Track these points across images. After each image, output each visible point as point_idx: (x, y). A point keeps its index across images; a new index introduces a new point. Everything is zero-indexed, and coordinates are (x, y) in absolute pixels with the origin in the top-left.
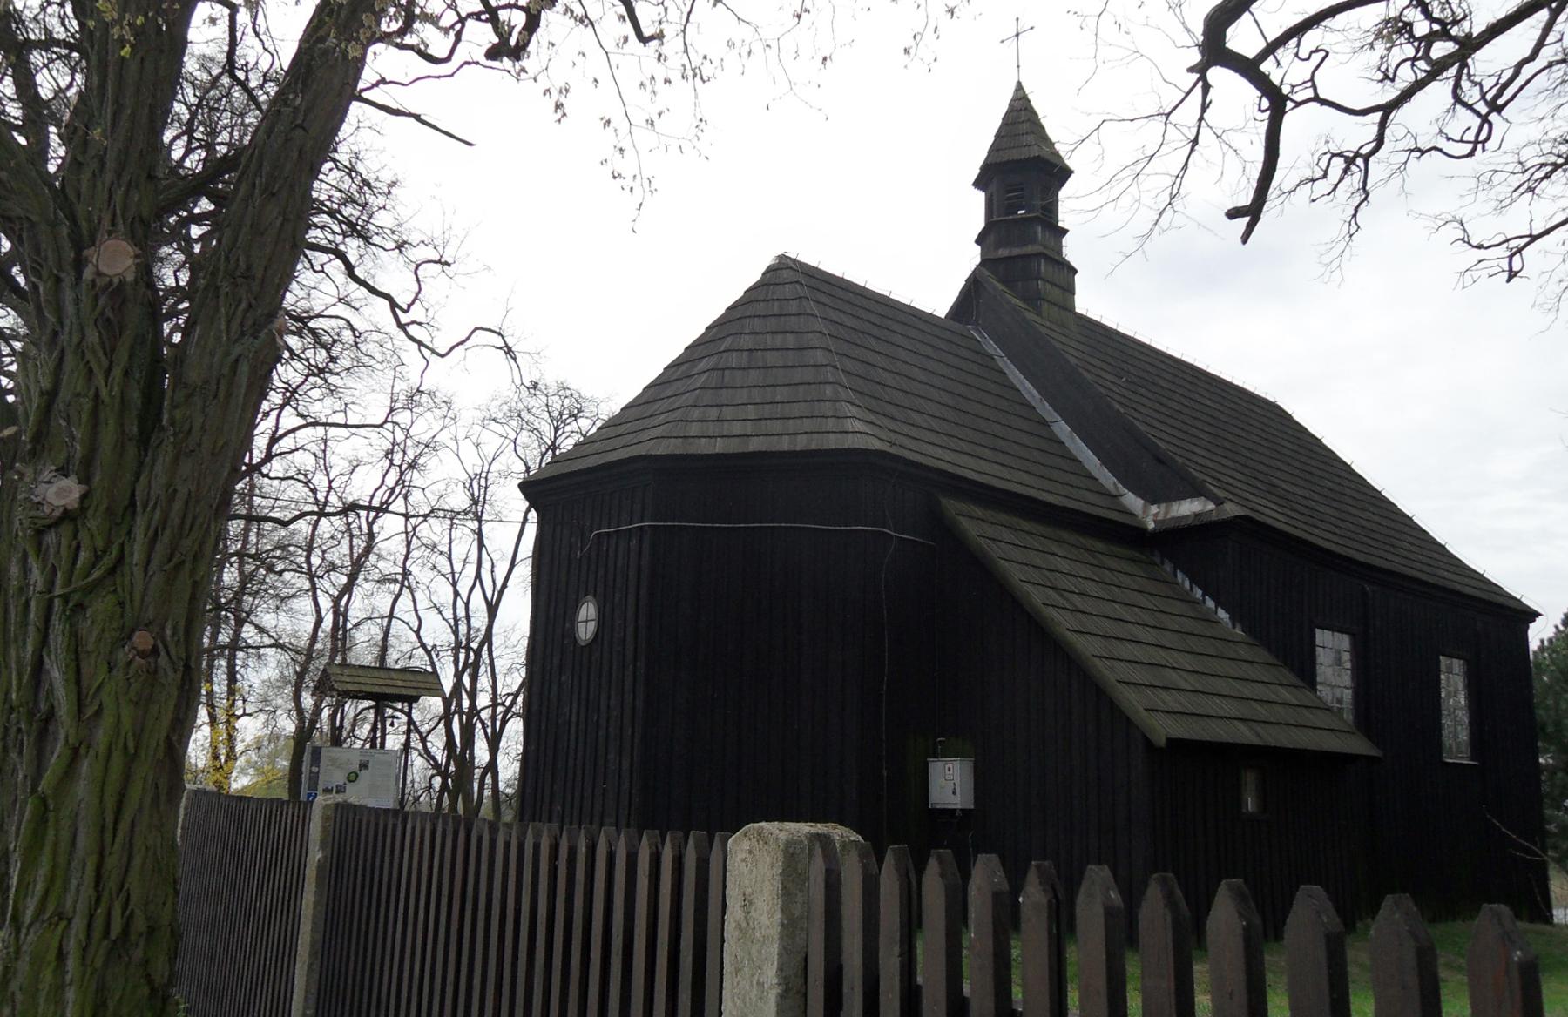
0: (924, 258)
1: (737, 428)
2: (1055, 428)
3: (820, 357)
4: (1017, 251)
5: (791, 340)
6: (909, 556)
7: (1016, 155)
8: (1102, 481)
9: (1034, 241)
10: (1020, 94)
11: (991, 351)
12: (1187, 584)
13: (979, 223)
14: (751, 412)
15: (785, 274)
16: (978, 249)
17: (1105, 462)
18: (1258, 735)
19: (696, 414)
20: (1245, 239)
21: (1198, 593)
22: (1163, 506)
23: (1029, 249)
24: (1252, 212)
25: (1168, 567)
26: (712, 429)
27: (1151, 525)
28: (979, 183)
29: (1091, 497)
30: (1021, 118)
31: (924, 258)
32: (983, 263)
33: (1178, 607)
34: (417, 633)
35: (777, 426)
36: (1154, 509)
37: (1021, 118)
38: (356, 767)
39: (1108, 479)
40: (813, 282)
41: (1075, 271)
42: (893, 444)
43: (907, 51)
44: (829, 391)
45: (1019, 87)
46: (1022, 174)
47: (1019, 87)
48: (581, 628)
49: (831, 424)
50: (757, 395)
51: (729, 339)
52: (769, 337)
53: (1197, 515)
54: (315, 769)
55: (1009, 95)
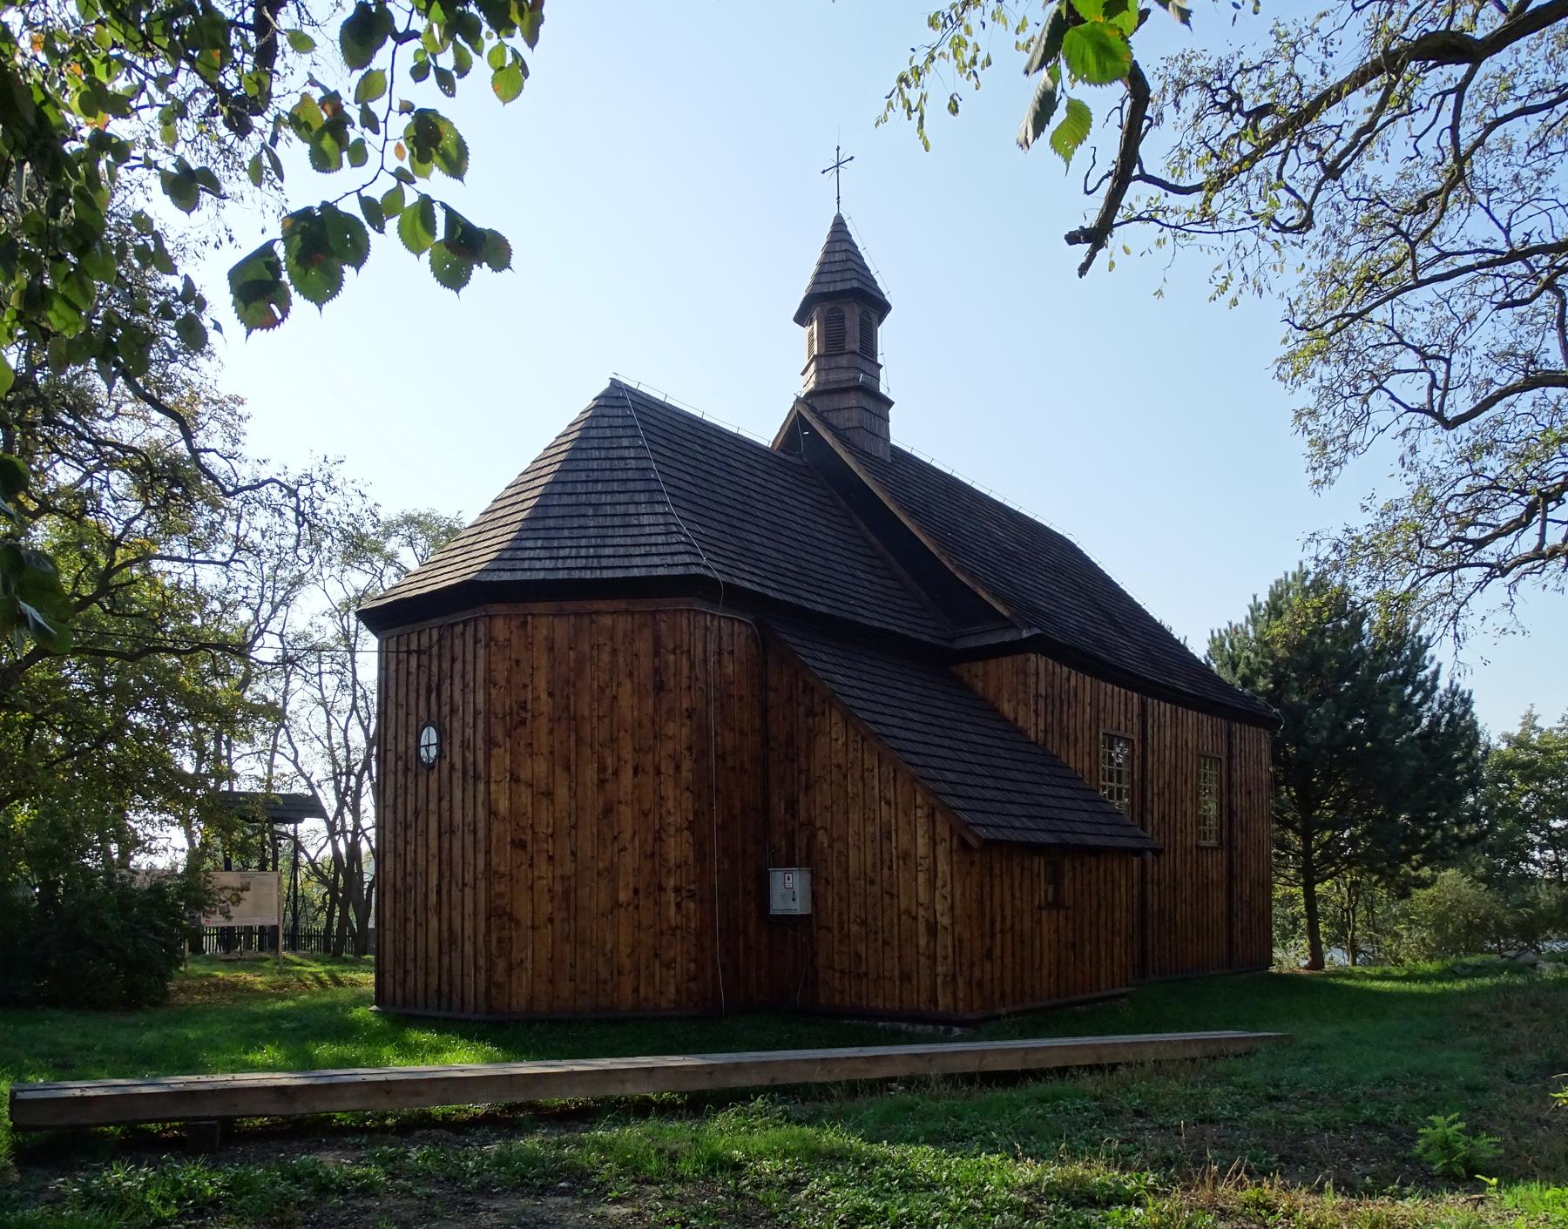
6: (779, 653)
20: (1083, 270)
24: (1095, 237)
28: (802, 318)
31: (751, 387)
34: (295, 762)
43: (1159, 293)
46: (845, 304)
47: (839, 230)
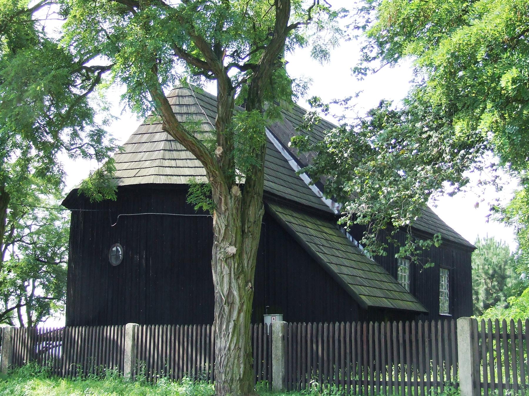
2: (290, 162)
12: (351, 239)
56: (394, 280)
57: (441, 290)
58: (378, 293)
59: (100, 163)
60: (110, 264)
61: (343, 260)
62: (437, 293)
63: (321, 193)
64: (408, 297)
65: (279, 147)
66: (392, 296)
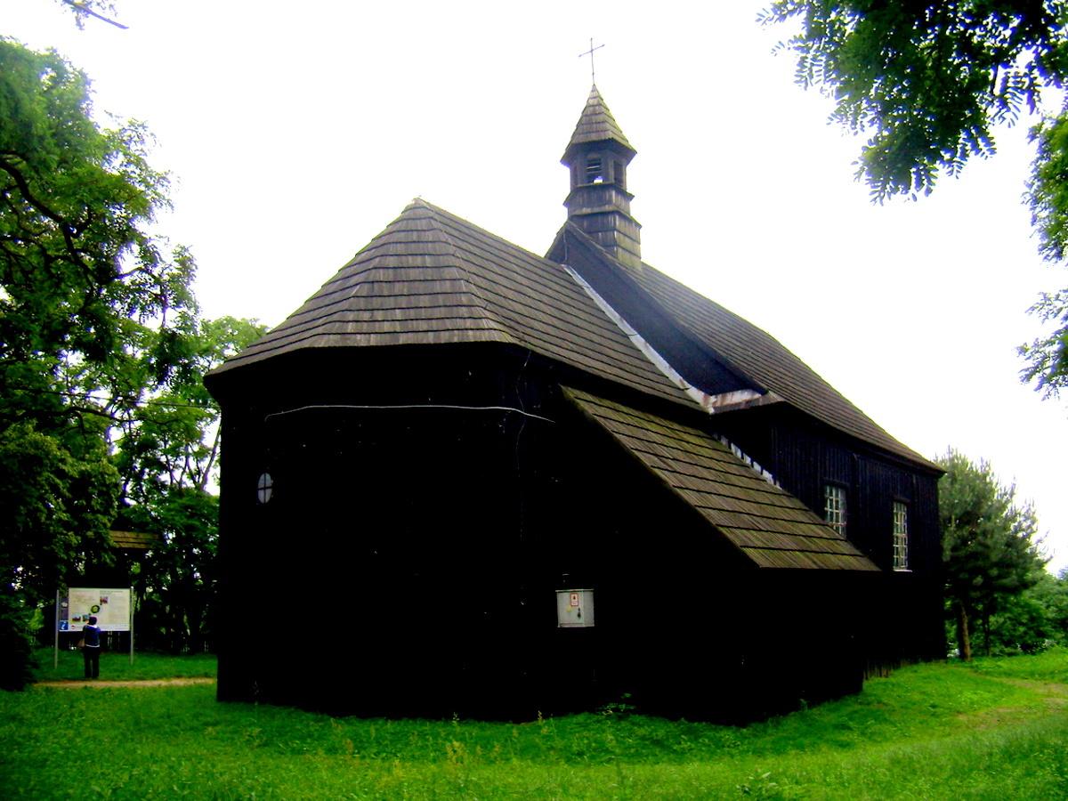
0: (527, 211)
1: (387, 327)
2: (633, 339)
3: (455, 273)
4: (596, 210)
5: (428, 261)
7: (594, 137)
8: (671, 378)
9: (610, 202)
10: (595, 94)
11: (580, 283)
12: (739, 454)
13: (566, 189)
14: (398, 314)
15: (420, 212)
16: (565, 210)
17: (673, 365)
18: (815, 563)
19: (351, 316)
21: (748, 460)
22: (720, 396)
23: (607, 208)
25: (724, 442)
26: (365, 327)
27: (711, 411)
29: (668, 390)
30: (595, 114)
31: (527, 211)
32: (572, 218)
33: (733, 469)
35: (423, 325)
36: (712, 399)
37: (595, 114)
38: (97, 602)
39: (675, 377)
40: (446, 221)
41: (640, 226)
42: (521, 340)
44: (464, 299)
45: (594, 89)
46: (598, 156)
47: (594, 89)
48: (261, 494)
49: (469, 323)
50: (403, 302)
51: (377, 260)
52: (410, 258)
53: (748, 402)
54: (64, 604)
55: (588, 94)
56: (819, 520)
57: (895, 534)
58: (787, 542)
59: (772, 7)
60: (139, 574)
61: (717, 485)
62: (890, 539)
63: (685, 382)
64: (845, 547)
65: (615, 317)
66: (814, 547)
